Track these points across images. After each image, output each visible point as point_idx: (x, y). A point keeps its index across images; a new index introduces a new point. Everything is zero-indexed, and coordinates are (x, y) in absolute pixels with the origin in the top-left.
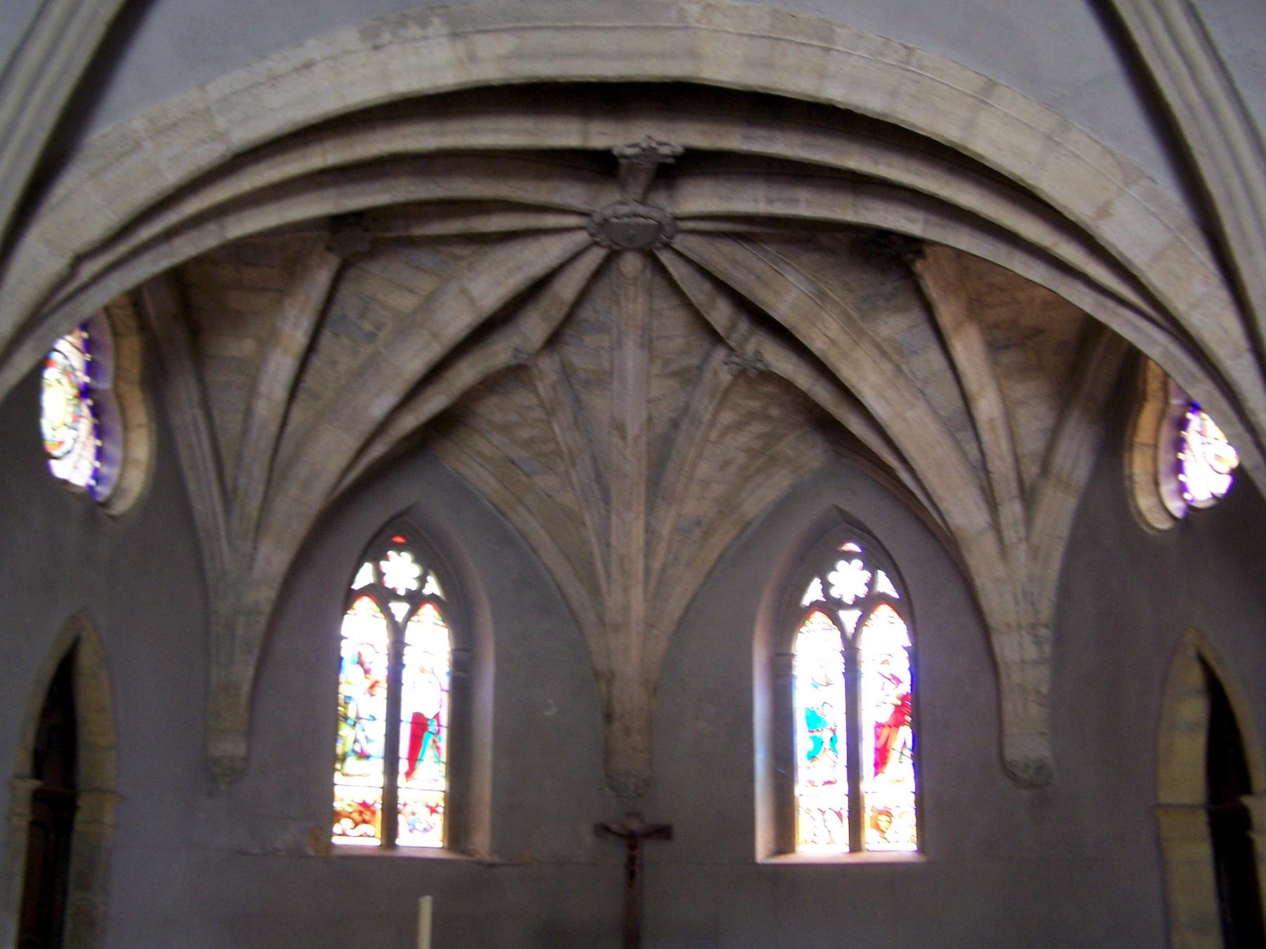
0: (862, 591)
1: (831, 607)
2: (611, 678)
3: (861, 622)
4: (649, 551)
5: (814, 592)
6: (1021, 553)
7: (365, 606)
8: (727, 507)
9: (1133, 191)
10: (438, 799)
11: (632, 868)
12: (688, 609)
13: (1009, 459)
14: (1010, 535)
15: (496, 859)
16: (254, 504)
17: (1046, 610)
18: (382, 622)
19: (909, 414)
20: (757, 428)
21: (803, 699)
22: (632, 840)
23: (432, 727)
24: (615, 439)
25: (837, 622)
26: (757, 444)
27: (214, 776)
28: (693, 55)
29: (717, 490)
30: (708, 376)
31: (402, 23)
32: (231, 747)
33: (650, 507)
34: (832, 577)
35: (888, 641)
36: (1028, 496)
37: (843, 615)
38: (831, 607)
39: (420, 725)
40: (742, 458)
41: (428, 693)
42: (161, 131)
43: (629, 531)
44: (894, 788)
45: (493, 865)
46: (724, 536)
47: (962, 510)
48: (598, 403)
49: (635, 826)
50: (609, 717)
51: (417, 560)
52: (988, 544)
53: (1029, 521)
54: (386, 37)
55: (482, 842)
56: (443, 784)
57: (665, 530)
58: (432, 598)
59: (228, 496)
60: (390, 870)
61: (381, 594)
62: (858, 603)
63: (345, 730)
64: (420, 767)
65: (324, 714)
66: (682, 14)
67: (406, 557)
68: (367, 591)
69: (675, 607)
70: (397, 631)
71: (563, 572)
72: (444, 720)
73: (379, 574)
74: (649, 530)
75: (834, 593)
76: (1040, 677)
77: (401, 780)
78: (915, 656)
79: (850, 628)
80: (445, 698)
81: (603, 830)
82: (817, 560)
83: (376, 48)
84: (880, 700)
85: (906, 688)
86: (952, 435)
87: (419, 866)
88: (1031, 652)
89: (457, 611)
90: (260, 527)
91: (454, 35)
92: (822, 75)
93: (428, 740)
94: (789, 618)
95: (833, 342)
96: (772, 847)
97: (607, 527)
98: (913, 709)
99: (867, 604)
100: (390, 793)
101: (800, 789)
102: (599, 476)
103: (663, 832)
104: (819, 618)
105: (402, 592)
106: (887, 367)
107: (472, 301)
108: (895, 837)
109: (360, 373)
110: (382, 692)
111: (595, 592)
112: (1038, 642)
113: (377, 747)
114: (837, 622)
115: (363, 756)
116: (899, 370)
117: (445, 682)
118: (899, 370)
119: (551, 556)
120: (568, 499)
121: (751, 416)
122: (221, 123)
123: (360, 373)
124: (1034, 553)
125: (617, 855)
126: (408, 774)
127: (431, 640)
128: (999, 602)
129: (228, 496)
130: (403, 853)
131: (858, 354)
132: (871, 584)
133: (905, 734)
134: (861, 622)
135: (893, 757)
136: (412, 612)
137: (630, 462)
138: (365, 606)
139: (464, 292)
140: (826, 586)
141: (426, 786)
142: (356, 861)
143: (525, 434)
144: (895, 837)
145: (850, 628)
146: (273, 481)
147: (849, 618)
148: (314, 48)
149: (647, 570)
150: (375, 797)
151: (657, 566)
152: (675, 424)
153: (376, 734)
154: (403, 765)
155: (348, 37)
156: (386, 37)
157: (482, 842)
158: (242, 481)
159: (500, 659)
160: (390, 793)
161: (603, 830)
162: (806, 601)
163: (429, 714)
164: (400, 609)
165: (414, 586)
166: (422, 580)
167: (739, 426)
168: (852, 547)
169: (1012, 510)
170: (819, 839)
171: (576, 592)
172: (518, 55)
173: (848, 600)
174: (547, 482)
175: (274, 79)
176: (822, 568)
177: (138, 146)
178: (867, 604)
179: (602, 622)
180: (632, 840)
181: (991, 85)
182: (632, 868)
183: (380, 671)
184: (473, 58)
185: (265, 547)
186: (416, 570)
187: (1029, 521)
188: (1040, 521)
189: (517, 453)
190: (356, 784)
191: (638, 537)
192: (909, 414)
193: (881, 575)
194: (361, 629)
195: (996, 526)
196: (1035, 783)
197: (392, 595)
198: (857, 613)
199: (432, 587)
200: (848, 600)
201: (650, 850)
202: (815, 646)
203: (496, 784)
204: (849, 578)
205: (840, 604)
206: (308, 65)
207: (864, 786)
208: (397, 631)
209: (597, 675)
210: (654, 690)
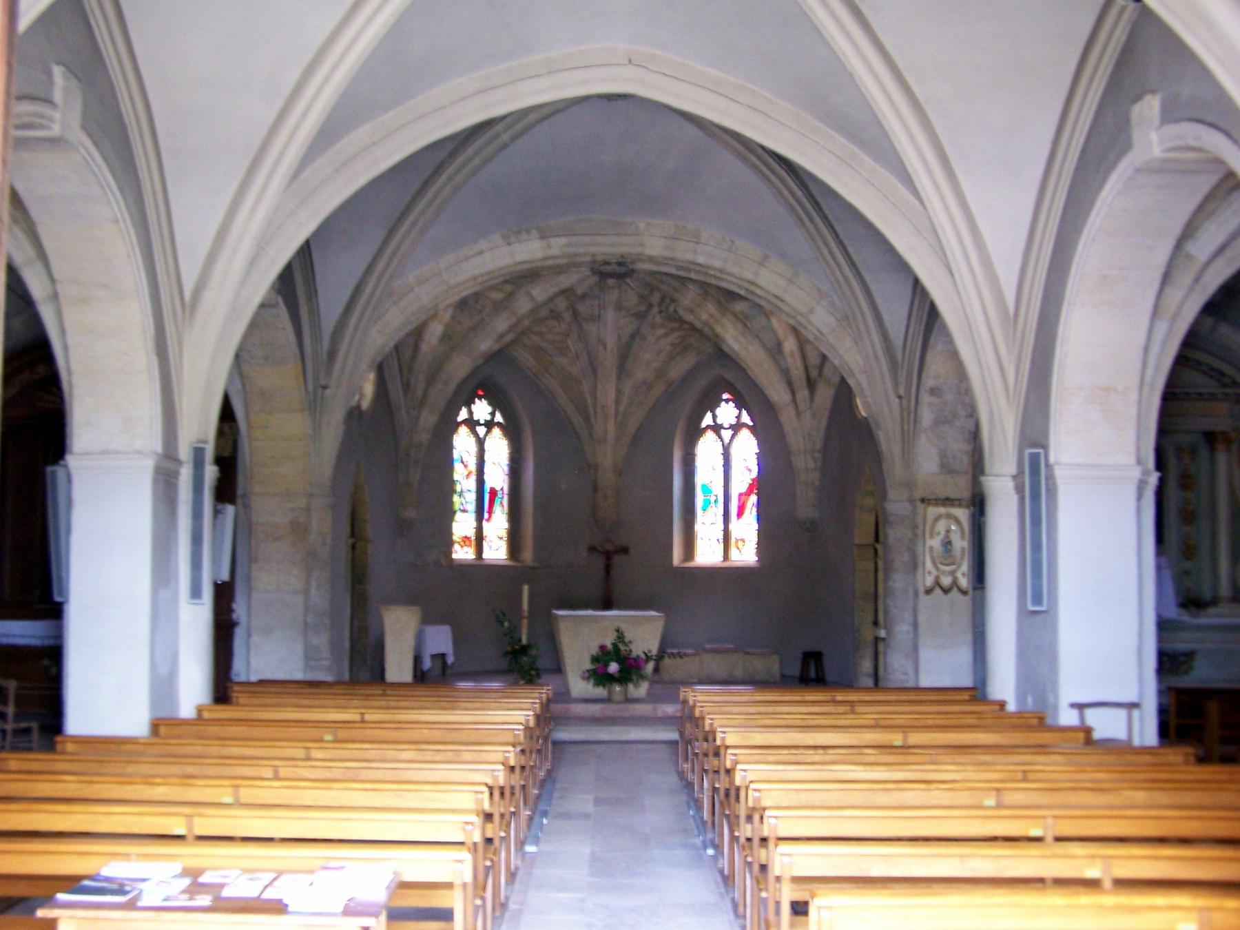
0: (734, 421)
1: (717, 428)
2: (596, 467)
3: (733, 437)
4: (618, 402)
5: (707, 420)
6: (808, 415)
7: (463, 430)
8: (660, 374)
9: (824, 303)
10: (504, 534)
11: (608, 569)
12: (638, 430)
13: (801, 369)
14: (802, 407)
15: (536, 565)
16: (420, 392)
17: (819, 443)
18: (473, 440)
19: (751, 348)
20: (676, 334)
21: (700, 478)
22: (608, 555)
23: (499, 493)
24: (601, 348)
25: (720, 437)
26: (677, 341)
27: (402, 527)
28: (642, 245)
29: (655, 365)
30: (650, 317)
31: (519, 232)
32: (410, 513)
33: (619, 378)
34: (731, 404)
35: (746, 448)
36: (811, 384)
37: (723, 432)
38: (717, 428)
39: (493, 493)
40: (669, 348)
41: (497, 477)
42: (422, 282)
43: (607, 393)
44: (747, 529)
45: (534, 568)
46: (659, 390)
47: (778, 393)
48: (592, 329)
49: (609, 547)
50: (595, 489)
51: (490, 404)
52: (791, 411)
53: (812, 399)
54: (513, 239)
55: (528, 555)
56: (506, 525)
57: (627, 390)
58: (499, 424)
59: (407, 387)
60: (479, 568)
61: (471, 423)
62: (731, 427)
63: (456, 498)
64: (494, 516)
65: (447, 487)
66: (637, 228)
67: (484, 402)
68: (465, 422)
69: (631, 428)
70: (481, 443)
71: (569, 408)
72: (506, 490)
73: (471, 413)
74: (619, 391)
75: (719, 421)
76: (815, 477)
77: (485, 523)
78: (760, 457)
79: (727, 441)
80: (506, 478)
81: (592, 549)
82: (711, 403)
83: (509, 244)
84: (740, 483)
85: (754, 474)
86: (773, 357)
87: (494, 568)
88: (811, 465)
89: (512, 432)
90: (422, 404)
91: (542, 238)
92: (695, 252)
93: (497, 501)
94: (694, 433)
95: (711, 316)
96: (682, 557)
97: (595, 387)
98: (758, 486)
99: (736, 427)
100: (479, 530)
101: (698, 527)
102: (591, 362)
103: (624, 550)
104: (710, 435)
105: (482, 422)
106: (740, 326)
107: (532, 299)
108: (746, 554)
109: (474, 328)
110: (473, 477)
111: (587, 420)
112: (815, 461)
113: (471, 507)
114: (720, 437)
115: (464, 511)
116: (745, 325)
117: (506, 469)
118: (745, 325)
119: (563, 400)
120: (575, 371)
121: (673, 330)
122: (445, 277)
123: (474, 328)
124: (814, 415)
125: (599, 562)
126: (488, 520)
127: (498, 448)
128: (796, 441)
129: (407, 387)
130: (488, 562)
131: (724, 321)
132: (738, 417)
133: (753, 498)
134: (733, 437)
135: (747, 511)
136: (488, 432)
137: (609, 359)
138: (463, 430)
139: (529, 294)
140: (714, 417)
141: (498, 526)
142: (463, 567)
143: (550, 337)
144: (746, 554)
145: (727, 441)
146: (431, 379)
147: (727, 434)
148: (483, 244)
149: (617, 411)
150: (471, 533)
151: (622, 409)
152: (632, 337)
153: (471, 497)
154: (486, 515)
155: (497, 238)
156: (513, 239)
157: (528, 555)
158: (413, 381)
159: (536, 455)
160: (479, 530)
161: (592, 549)
162: (704, 425)
163: (498, 489)
164: (481, 430)
165: (489, 418)
166: (493, 414)
167: (666, 335)
168: (725, 396)
169: (803, 393)
170: (707, 553)
171: (577, 420)
172: (569, 245)
173: (726, 426)
174: (562, 361)
175: (467, 258)
176: (713, 405)
177: (412, 289)
178: (736, 427)
179: (591, 436)
180: (608, 555)
181: (767, 257)
182: (608, 569)
183: (473, 467)
184: (549, 246)
185: (425, 413)
186: (490, 409)
187: (812, 399)
188: (817, 399)
189: (544, 345)
190: (463, 525)
191: (612, 395)
192: (751, 348)
193: (744, 412)
194: (463, 443)
195: (794, 401)
196: (811, 527)
197: (478, 423)
198: (730, 432)
199: (499, 418)
200: (726, 426)
201: (617, 559)
202: (707, 450)
203: (535, 524)
204: (727, 412)
205: (721, 427)
206: (481, 252)
207: (731, 527)
208: (481, 443)
209: (589, 465)
210: (619, 473)
